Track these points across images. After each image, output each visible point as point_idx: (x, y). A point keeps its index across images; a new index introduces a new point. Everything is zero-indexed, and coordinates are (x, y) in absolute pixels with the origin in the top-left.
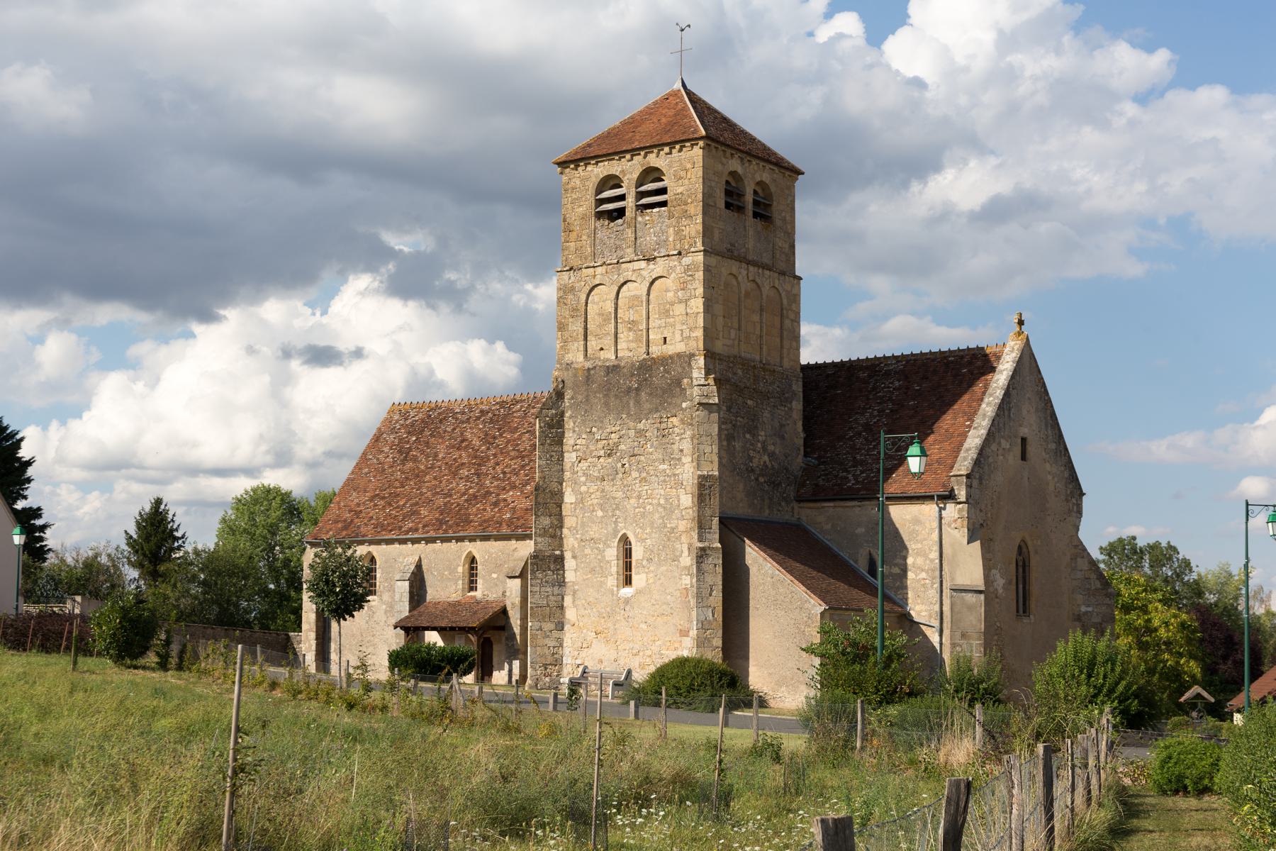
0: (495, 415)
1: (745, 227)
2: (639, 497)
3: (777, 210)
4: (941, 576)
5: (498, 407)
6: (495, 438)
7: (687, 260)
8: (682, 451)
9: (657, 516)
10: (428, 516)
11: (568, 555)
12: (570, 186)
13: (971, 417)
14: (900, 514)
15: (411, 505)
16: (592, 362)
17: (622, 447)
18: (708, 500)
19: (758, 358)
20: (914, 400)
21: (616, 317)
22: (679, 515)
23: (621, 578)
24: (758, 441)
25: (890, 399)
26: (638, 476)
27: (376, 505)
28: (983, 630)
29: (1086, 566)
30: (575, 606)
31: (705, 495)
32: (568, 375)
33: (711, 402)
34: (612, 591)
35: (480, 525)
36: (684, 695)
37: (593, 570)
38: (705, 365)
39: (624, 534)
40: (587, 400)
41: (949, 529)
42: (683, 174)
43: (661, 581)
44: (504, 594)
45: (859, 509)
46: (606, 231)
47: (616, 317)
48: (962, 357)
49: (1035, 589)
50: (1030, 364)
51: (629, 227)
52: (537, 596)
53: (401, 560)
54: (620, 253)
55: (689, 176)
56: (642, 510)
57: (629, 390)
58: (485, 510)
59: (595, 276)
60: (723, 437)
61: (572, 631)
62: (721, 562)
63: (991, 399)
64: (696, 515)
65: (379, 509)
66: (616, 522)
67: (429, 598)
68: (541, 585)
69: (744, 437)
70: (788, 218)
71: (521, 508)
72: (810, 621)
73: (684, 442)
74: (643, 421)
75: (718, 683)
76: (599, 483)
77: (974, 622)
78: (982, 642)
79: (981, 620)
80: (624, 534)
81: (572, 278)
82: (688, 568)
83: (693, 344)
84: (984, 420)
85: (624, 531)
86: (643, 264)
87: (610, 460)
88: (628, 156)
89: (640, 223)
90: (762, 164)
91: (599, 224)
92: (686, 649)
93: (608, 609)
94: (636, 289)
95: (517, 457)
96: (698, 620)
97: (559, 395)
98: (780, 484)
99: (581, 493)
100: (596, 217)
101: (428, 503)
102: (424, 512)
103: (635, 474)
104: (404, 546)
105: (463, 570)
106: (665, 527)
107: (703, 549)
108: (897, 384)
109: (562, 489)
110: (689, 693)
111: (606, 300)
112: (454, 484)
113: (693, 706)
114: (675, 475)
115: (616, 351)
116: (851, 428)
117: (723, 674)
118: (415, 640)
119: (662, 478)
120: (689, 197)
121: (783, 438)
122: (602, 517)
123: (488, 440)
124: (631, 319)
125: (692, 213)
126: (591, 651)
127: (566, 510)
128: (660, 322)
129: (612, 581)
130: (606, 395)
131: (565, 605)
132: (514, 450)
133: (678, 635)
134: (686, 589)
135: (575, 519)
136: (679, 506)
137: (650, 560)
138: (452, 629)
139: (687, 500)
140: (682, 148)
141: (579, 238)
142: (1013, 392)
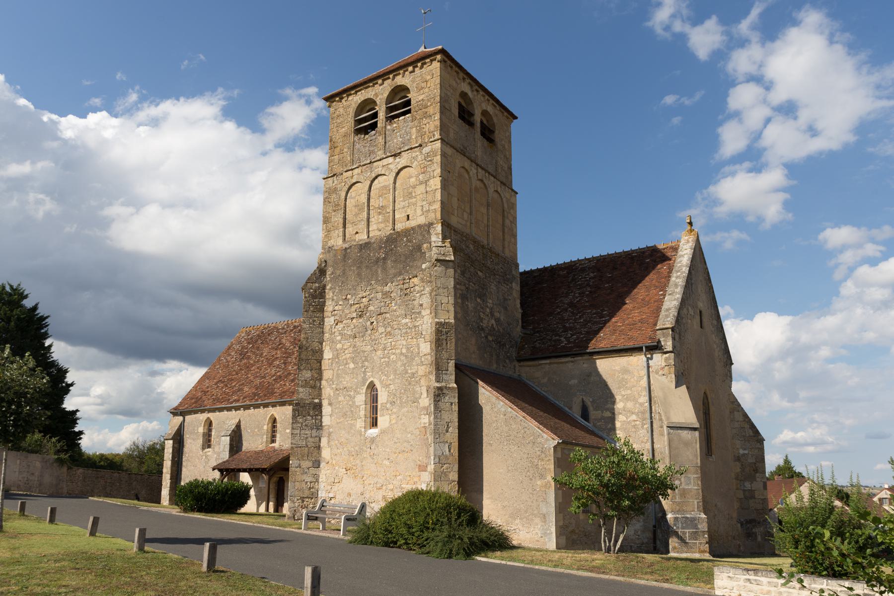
1: (474, 139)
2: (384, 349)
3: (498, 135)
4: (651, 418)
7: (426, 150)
8: (421, 305)
9: (400, 363)
11: (325, 403)
12: (336, 115)
13: (663, 287)
14: (606, 366)
15: (239, 385)
16: (348, 243)
17: (371, 308)
18: (445, 344)
19: (485, 242)
20: (608, 283)
21: (369, 206)
22: (419, 362)
23: (369, 420)
24: (487, 307)
25: (588, 285)
26: (383, 331)
27: (218, 387)
28: (699, 465)
29: (741, 419)
30: (329, 446)
31: (443, 339)
33: (447, 259)
36: (416, 534)
38: (442, 231)
39: (372, 382)
40: (344, 274)
41: (657, 376)
42: (424, 85)
46: (362, 143)
47: (369, 206)
48: (644, 253)
49: (714, 434)
50: (700, 255)
52: (297, 438)
54: (372, 156)
55: (428, 86)
56: (386, 359)
58: (285, 385)
59: (353, 176)
60: (458, 295)
62: (457, 401)
63: (679, 274)
64: (434, 358)
66: (365, 372)
67: (244, 449)
68: (301, 429)
69: (476, 300)
70: (506, 147)
72: (543, 455)
73: (424, 298)
75: (456, 520)
77: (691, 458)
78: (700, 475)
79: (697, 455)
80: (372, 382)
81: (336, 182)
82: (426, 408)
83: (432, 216)
84: (677, 288)
85: (371, 379)
86: (391, 160)
87: (361, 320)
88: (380, 81)
89: (389, 130)
90: (487, 97)
91: (356, 138)
92: (424, 482)
93: (357, 448)
94: (385, 181)
96: (435, 455)
97: (321, 272)
98: (504, 345)
99: (337, 350)
100: (354, 133)
101: (250, 383)
102: (246, 389)
104: (230, 412)
106: (407, 373)
107: (440, 389)
108: (592, 275)
109: (322, 348)
110: (422, 531)
113: (426, 549)
114: (415, 327)
115: (368, 232)
116: (557, 307)
117: (462, 510)
119: (404, 331)
120: (428, 100)
121: (506, 309)
122: (353, 369)
124: (381, 205)
125: (431, 114)
126: (341, 485)
127: (325, 364)
129: (360, 424)
130: (359, 267)
131: (322, 445)
133: (417, 469)
134: (425, 427)
135: (332, 371)
136: (419, 353)
138: (257, 470)
139: (426, 347)
140: (423, 64)
141: (341, 152)
142: (693, 272)
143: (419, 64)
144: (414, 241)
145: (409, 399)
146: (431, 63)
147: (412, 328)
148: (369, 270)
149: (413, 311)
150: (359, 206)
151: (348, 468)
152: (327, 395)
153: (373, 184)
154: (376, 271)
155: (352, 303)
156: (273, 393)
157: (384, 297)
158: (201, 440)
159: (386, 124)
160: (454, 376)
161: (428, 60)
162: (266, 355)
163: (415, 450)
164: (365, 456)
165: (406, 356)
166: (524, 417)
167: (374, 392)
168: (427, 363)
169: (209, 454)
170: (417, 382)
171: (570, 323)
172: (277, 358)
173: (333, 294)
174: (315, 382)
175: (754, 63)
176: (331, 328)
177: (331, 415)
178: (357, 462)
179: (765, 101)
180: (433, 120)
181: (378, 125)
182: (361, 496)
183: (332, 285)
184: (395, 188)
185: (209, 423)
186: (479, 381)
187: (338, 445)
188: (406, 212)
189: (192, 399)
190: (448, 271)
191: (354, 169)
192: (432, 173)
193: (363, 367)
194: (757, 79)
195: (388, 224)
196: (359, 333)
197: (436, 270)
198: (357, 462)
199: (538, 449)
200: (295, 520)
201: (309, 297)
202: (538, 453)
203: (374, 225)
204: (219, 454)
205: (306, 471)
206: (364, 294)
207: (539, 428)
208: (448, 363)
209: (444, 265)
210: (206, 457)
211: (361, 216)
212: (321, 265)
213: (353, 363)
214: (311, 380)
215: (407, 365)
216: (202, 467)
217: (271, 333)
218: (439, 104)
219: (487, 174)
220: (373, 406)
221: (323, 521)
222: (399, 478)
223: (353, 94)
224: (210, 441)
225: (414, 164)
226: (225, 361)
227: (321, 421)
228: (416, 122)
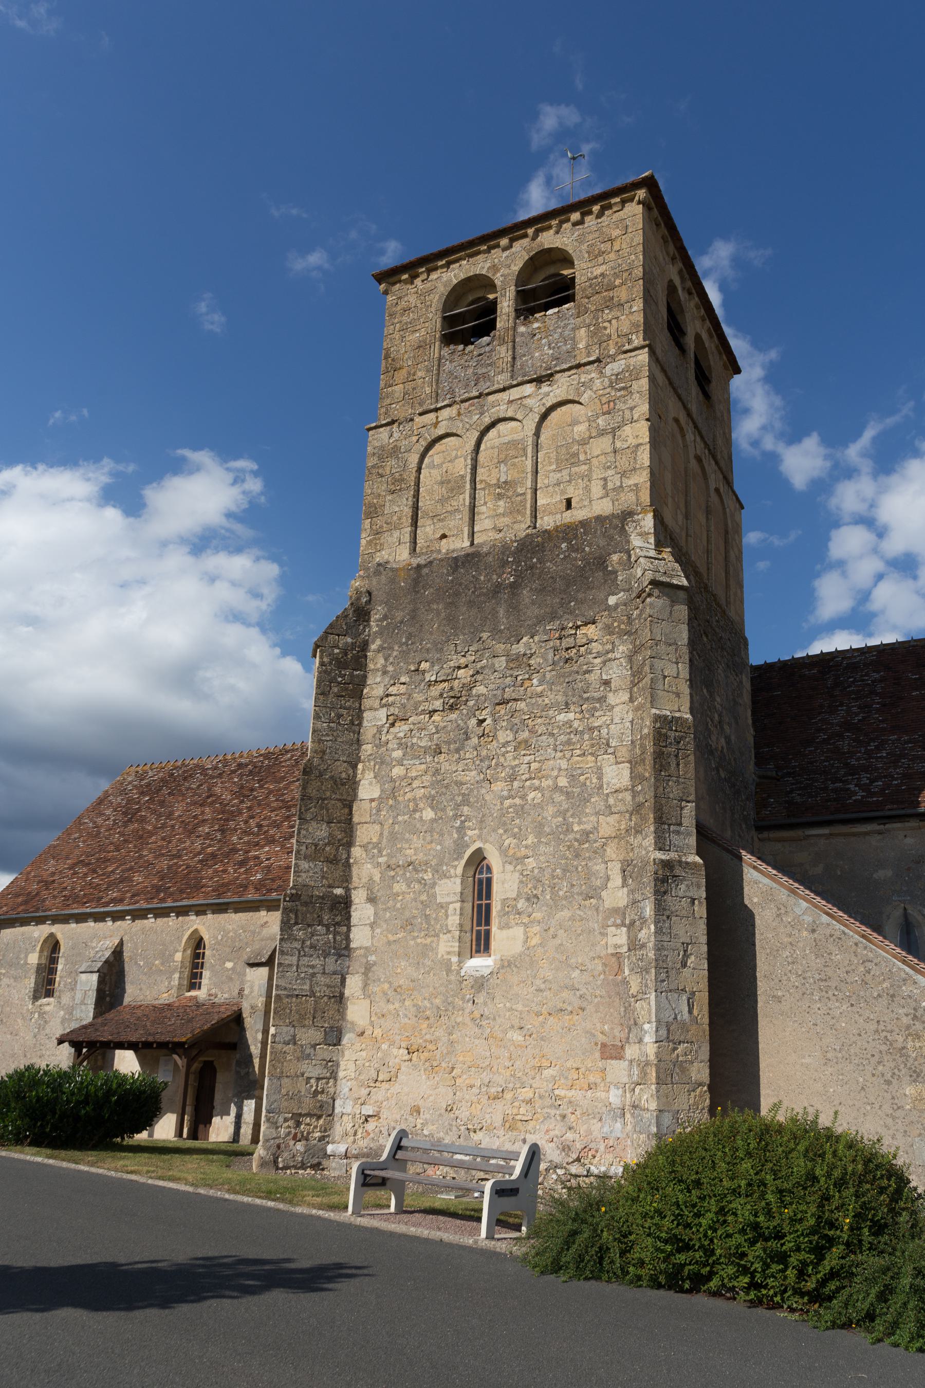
0: (256, 767)
2: (512, 778)
5: (261, 759)
6: (252, 790)
9: (551, 810)
10: (142, 882)
11: (359, 897)
12: (399, 308)
15: (123, 871)
17: (480, 689)
18: (673, 765)
21: (474, 481)
22: (601, 806)
26: (510, 738)
27: (75, 873)
32: (379, 583)
33: (675, 582)
34: (448, 964)
35: (213, 891)
37: (409, 924)
39: (479, 851)
40: (413, 618)
43: (558, 941)
44: (241, 992)
45: (879, 837)
47: (474, 481)
51: (503, 342)
53: (94, 945)
55: (616, 247)
57: (497, 589)
59: (437, 423)
61: (357, 1046)
62: (704, 895)
65: (78, 878)
66: (461, 830)
67: (127, 1000)
68: (301, 953)
71: (280, 866)
74: (525, 639)
76: (429, 759)
81: (396, 435)
83: (627, 500)
85: (478, 845)
86: (529, 389)
87: (453, 716)
88: (504, 242)
89: (522, 335)
91: (446, 352)
93: (437, 1001)
95: (281, 808)
96: (658, 1021)
99: (392, 780)
100: (442, 342)
102: (138, 878)
103: (504, 736)
104: (101, 924)
105: (183, 958)
106: (569, 830)
108: (876, 676)
109: (355, 775)
111: (456, 457)
112: (188, 844)
114: (591, 729)
115: (472, 534)
118: (99, 1063)
120: (616, 276)
122: (433, 821)
123: (242, 793)
124: (502, 480)
126: (395, 1088)
127: (361, 812)
128: (559, 475)
131: (347, 993)
132: (276, 800)
133: (597, 1055)
135: (377, 827)
136: (601, 787)
137: (533, 899)
138: (163, 1045)
140: (603, 209)
141: (411, 377)
143: (596, 208)
144: (587, 549)
145: (576, 890)
146: (623, 207)
147: (582, 733)
148: (474, 611)
149: (585, 696)
150: (449, 481)
151: (415, 1047)
152: (364, 880)
153: (485, 438)
154: (494, 612)
155: (433, 678)
156: (198, 887)
157: (512, 665)
158: (33, 980)
159: (515, 323)
160: (695, 838)
161: (618, 200)
162: (180, 816)
163: (590, 1008)
164: (459, 1019)
165: (567, 793)
166: (863, 936)
167: (481, 873)
168: (623, 809)
169: (47, 1008)
170: (595, 852)
171: (858, 759)
172: (204, 821)
173: (386, 659)
174: (337, 849)
175: (864, 500)
176: (379, 732)
177: (373, 926)
178: (437, 1034)
179: (875, 551)
180: (627, 312)
181: (498, 325)
182: (446, 1115)
183: (384, 642)
184: (536, 447)
185: (52, 946)
186: (743, 853)
187: (391, 993)
188: (563, 492)
189: (17, 895)
190: (676, 607)
191: (441, 408)
192: (627, 413)
193: (456, 816)
194: (867, 521)
195: (519, 518)
196: (448, 743)
197: (651, 604)
198: (437, 1034)
199: (905, 1010)
200: (277, 1168)
201: (330, 663)
202: (906, 1020)
203: (487, 521)
204: (70, 1010)
205: (308, 1051)
206: (463, 661)
207: (904, 962)
208: (682, 809)
209: (667, 595)
210: (42, 1015)
211: (455, 503)
212: (358, 599)
213: (432, 808)
214: (329, 844)
215: (569, 814)
216: (29, 1037)
217: (190, 775)
218: (641, 282)
219: (707, 451)
220: (480, 906)
221: (399, 1189)
222: (547, 1073)
223: (442, 267)
224: (51, 982)
225: (585, 395)
226: (91, 825)
227: (348, 939)
228: (587, 318)
